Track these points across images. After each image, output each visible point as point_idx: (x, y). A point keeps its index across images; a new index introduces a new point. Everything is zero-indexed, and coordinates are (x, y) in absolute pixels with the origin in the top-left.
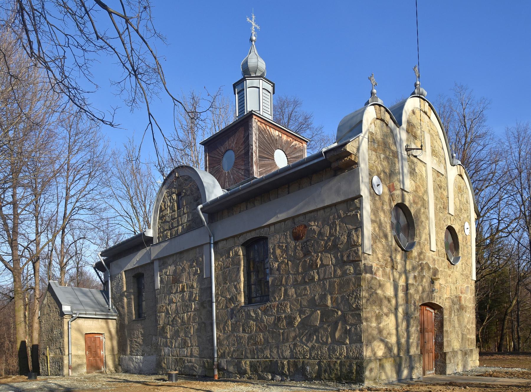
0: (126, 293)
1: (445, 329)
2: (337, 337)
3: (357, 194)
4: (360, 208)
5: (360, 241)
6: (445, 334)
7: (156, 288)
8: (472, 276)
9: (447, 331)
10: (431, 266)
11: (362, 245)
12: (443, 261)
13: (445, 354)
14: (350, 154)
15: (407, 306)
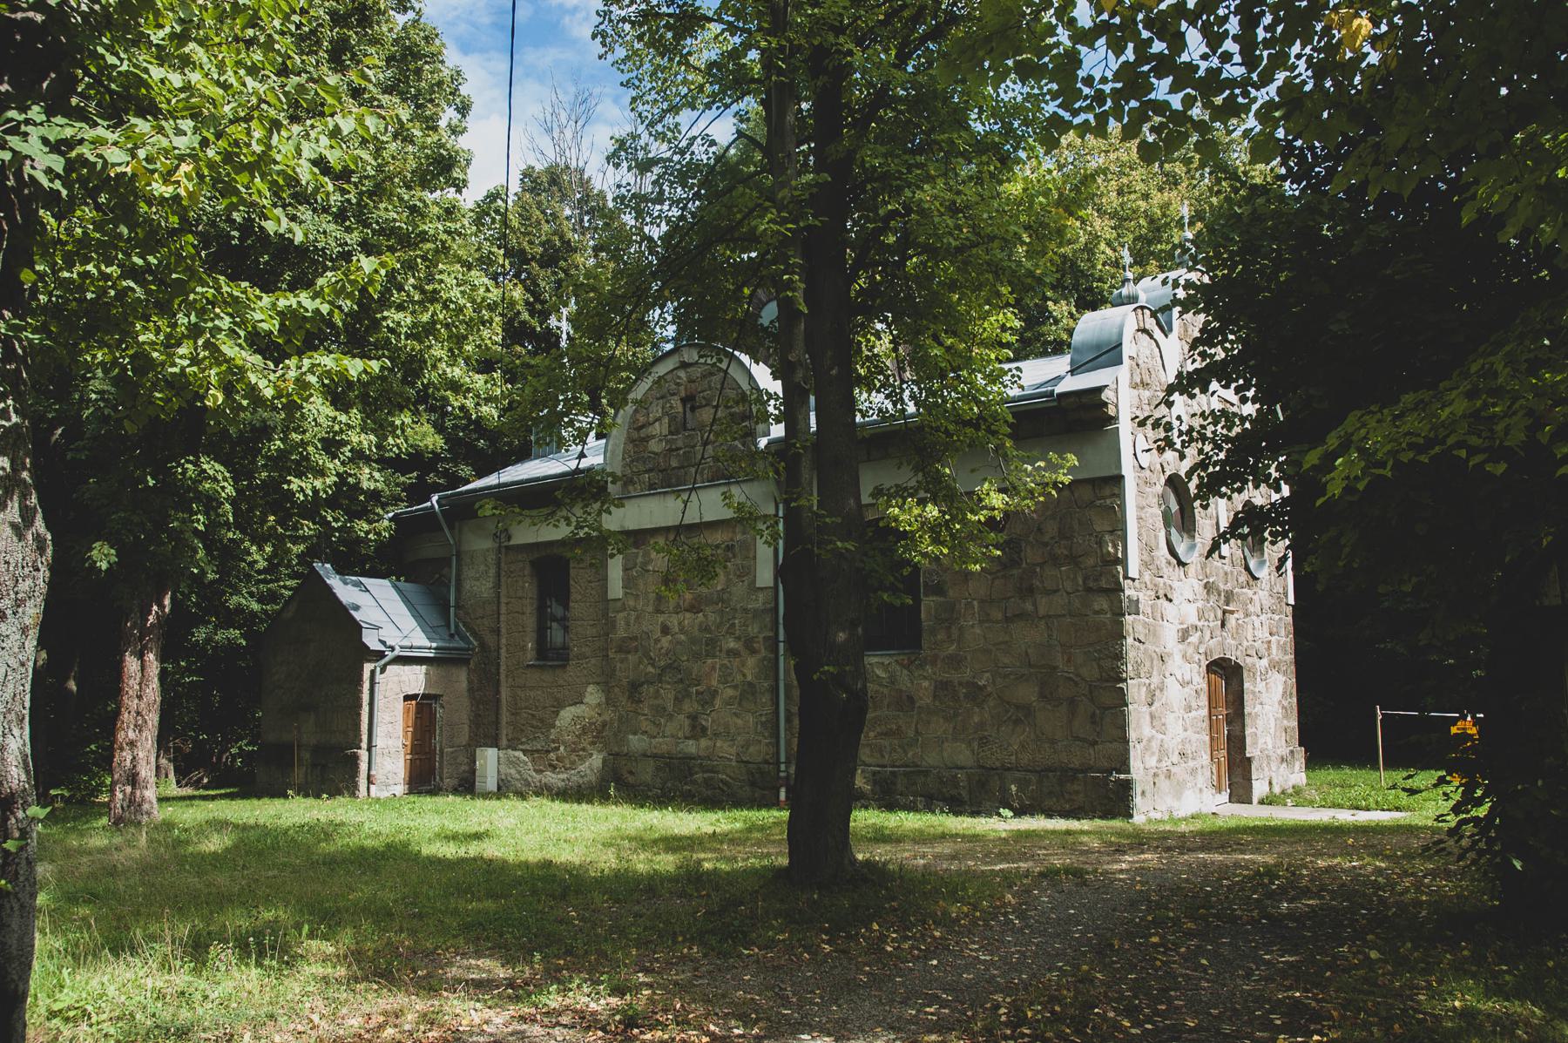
0: (103, 556)
1: (1247, 710)
2: (1505, 466)
3: (1116, 472)
4: (1121, 495)
5: (1120, 555)
6: (1248, 721)
7: (611, 595)
8: (1286, 597)
9: (1250, 714)
10: (1222, 587)
11: (1124, 562)
12: (1239, 573)
13: (1249, 760)
14: (1105, 404)
15: (870, 840)
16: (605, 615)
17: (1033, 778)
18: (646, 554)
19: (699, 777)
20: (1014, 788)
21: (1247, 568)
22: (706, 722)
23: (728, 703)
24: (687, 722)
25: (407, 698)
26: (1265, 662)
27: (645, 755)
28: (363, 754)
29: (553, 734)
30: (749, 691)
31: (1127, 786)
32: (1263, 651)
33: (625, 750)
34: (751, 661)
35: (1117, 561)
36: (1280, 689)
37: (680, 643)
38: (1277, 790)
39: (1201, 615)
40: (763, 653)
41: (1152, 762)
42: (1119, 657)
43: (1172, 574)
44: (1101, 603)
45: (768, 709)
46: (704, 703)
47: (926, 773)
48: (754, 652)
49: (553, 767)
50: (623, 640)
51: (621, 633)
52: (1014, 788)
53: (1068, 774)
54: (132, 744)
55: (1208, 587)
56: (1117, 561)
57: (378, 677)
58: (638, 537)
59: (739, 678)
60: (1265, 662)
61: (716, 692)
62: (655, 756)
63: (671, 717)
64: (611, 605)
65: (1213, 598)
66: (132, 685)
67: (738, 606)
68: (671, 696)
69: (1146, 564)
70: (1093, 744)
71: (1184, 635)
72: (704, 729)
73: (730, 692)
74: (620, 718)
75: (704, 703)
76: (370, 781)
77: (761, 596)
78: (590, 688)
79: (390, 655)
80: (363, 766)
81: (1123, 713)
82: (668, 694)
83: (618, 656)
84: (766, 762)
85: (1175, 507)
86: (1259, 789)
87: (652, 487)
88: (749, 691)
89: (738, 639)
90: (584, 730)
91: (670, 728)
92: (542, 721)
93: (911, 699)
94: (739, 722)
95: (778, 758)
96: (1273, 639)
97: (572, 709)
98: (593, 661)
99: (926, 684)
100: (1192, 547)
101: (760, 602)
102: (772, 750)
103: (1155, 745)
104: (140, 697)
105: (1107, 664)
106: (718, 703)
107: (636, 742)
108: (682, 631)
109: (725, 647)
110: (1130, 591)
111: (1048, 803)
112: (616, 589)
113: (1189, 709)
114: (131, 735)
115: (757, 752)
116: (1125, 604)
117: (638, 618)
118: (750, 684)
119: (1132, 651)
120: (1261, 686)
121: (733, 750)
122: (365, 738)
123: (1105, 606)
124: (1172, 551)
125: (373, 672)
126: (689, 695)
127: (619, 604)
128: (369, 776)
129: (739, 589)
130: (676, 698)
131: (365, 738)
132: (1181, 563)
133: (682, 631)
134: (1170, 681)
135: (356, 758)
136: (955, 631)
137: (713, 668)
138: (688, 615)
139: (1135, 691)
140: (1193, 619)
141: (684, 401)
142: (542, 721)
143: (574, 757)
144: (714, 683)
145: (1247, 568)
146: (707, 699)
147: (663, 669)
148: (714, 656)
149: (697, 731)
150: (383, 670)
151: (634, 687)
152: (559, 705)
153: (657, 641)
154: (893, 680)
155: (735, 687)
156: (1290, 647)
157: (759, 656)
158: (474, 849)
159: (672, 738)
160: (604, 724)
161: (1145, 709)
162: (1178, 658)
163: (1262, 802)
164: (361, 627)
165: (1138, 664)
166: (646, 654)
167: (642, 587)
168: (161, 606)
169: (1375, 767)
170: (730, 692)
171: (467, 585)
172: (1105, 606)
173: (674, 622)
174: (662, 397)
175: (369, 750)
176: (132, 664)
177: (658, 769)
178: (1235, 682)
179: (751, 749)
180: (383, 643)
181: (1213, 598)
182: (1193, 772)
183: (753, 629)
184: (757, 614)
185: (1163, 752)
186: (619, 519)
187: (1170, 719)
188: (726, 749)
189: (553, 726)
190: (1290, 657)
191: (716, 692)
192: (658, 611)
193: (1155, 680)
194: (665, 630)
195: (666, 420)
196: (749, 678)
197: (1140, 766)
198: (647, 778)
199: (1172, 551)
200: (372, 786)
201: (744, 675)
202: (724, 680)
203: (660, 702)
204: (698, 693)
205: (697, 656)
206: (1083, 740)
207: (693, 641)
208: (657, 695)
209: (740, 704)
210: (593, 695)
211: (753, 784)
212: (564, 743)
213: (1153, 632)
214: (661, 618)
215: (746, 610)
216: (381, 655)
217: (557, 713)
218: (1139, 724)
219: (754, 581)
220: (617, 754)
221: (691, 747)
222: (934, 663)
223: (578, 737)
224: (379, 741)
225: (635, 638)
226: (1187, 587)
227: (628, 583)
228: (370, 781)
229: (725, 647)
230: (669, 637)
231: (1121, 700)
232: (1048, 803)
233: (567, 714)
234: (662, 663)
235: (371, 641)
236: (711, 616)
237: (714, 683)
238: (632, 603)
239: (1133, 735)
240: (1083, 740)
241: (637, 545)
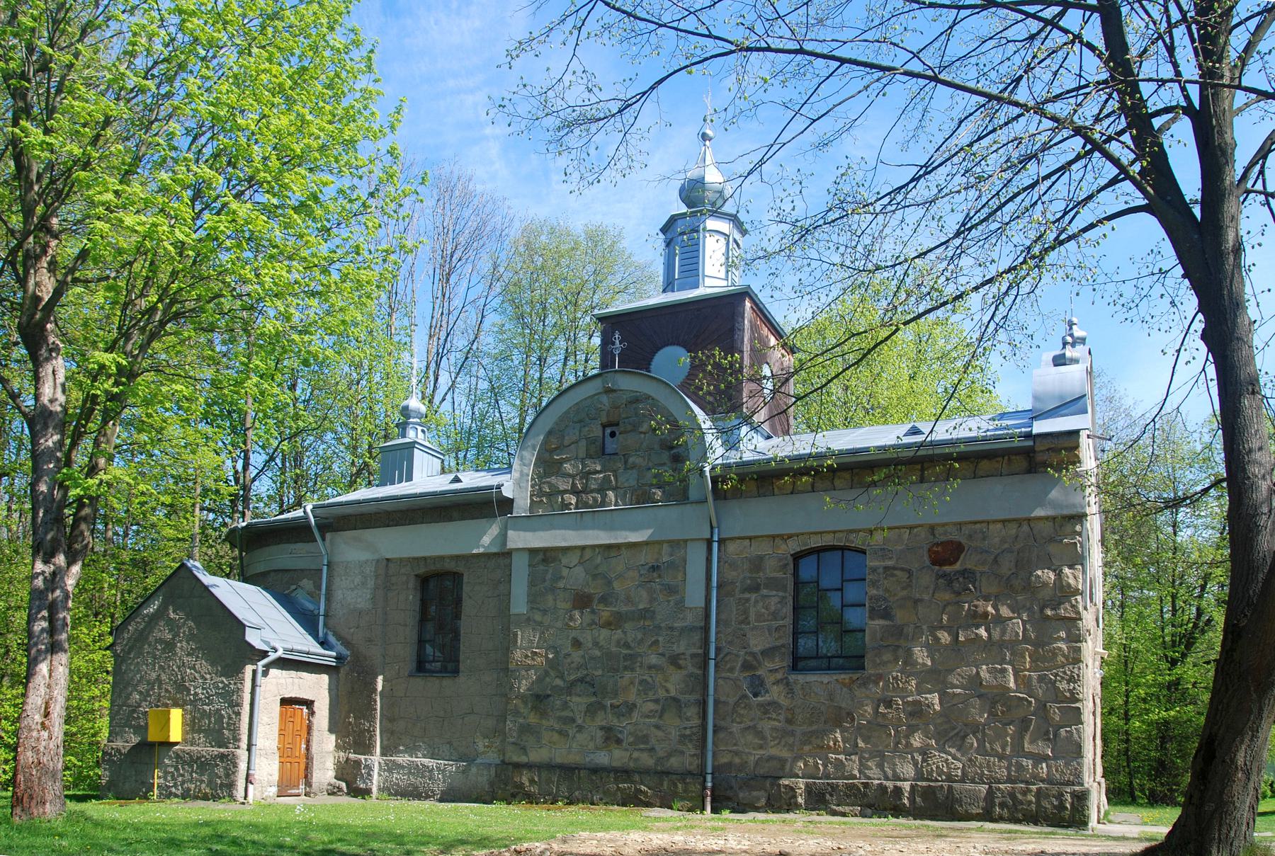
7: (514, 610)
24: (600, 734)
28: (242, 754)
40: (691, 669)
61: (634, 705)
67: (662, 625)
73: (651, 706)
79: (273, 656)
80: (243, 766)
102: (696, 762)
118: (675, 699)
122: (244, 738)
128: (248, 775)
131: (244, 738)
148: (633, 670)
150: (265, 674)
157: (684, 672)
158: (1098, 701)
164: (244, 626)
170: (651, 706)
171: (338, 595)
173: (587, 638)
174: (580, 421)
175: (249, 750)
183: (681, 647)
194: (577, 644)
195: (583, 443)
196: (673, 694)
201: (667, 691)
209: (660, 717)
216: (264, 654)
219: (682, 601)
227: (533, 599)
228: (248, 780)
230: (581, 652)
234: (572, 677)
235: (253, 638)
236: (631, 632)
241: (545, 561)
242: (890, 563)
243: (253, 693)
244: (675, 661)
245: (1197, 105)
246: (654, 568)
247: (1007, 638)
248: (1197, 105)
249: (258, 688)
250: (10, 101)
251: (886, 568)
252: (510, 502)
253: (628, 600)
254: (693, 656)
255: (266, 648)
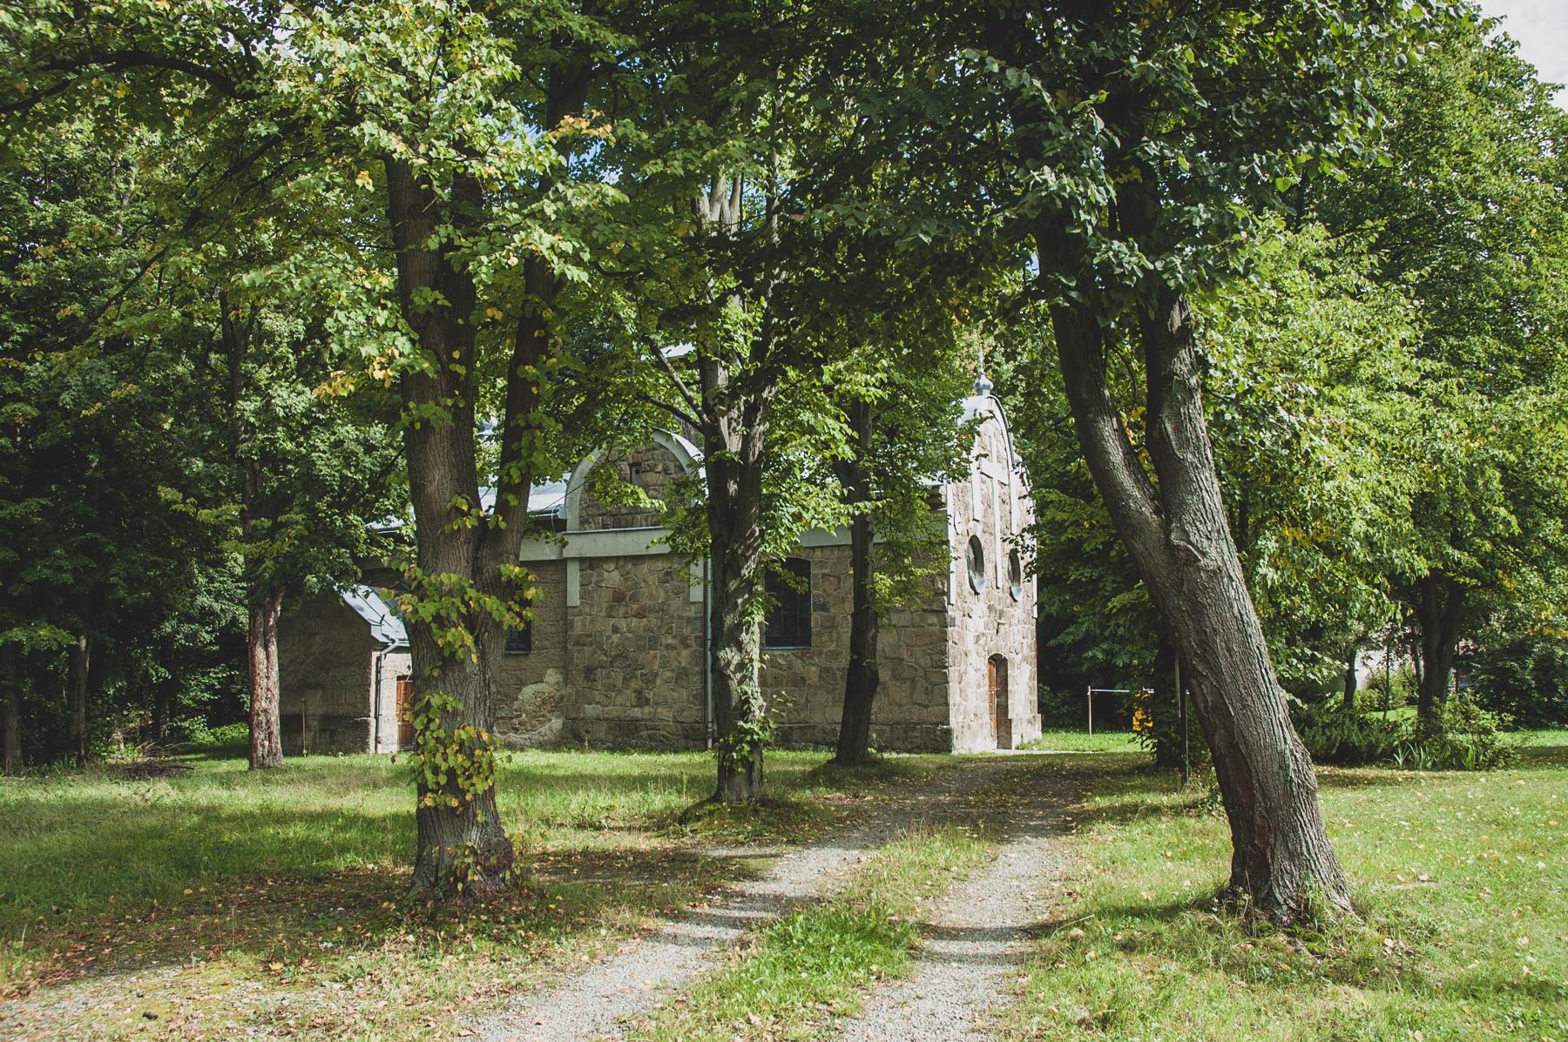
6: (1010, 695)
7: (569, 604)
11: (948, 594)
16: (565, 618)
17: (887, 728)
18: (601, 575)
19: (644, 733)
20: (874, 735)
21: (1011, 595)
22: (649, 695)
23: (666, 682)
24: (633, 695)
25: (399, 678)
26: (1020, 656)
27: (598, 719)
28: (372, 721)
29: (516, 705)
30: (682, 674)
31: (949, 732)
32: (1019, 650)
33: (582, 715)
34: (685, 653)
35: (944, 593)
36: (1028, 674)
37: (627, 639)
38: (1026, 741)
39: (986, 626)
40: (694, 647)
41: (960, 718)
42: (944, 653)
43: (971, 599)
44: (933, 619)
45: (699, 686)
46: (647, 682)
47: (814, 727)
48: (687, 646)
49: (516, 730)
50: (580, 636)
51: (578, 630)
52: (874, 735)
53: (910, 727)
54: (265, 711)
55: (990, 608)
56: (944, 593)
57: (384, 663)
58: (590, 563)
59: (675, 664)
60: (1020, 656)
61: (657, 674)
62: (607, 719)
63: (620, 692)
64: (569, 611)
65: (993, 615)
66: (262, 668)
68: (620, 677)
69: (959, 595)
70: (927, 707)
71: (978, 639)
72: (647, 701)
73: (668, 674)
74: (578, 692)
75: (647, 682)
76: (377, 741)
77: (693, 608)
78: (550, 671)
79: (392, 646)
80: (373, 730)
81: (946, 688)
82: (618, 676)
83: (576, 648)
84: (697, 722)
85: (972, 557)
86: (1016, 740)
87: (604, 526)
88: (682, 674)
89: (675, 637)
90: (544, 702)
91: (620, 699)
92: (506, 696)
93: (803, 679)
94: (676, 695)
95: (705, 716)
96: (1025, 641)
97: (534, 686)
98: (552, 651)
99: (814, 669)
100: (982, 582)
101: (692, 612)
103: (962, 708)
104: (268, 678)
105: (936, 657)
106: (658, 681)
107: (590, 710)
108: (629, 631)
109: (664, 642)
110: (951, 612)
111: (898, 744)
112: (574, 598)
113: (979, 686)
114: (264, 705)
115: (692, 714)
116: (949, 620)
117: (592, 621)
118: (684, 668)
119: (952, 649)
120: (1017, 671)
121: (671, 715)
123: (936, 621)
124: (972, 587)
125: (379, 659)
126: (635, 676)
127: (576, 610)
128: (377, 737)
129: (676, 603)
130: (624, 678)
132: (977, 593)
133: (629, 631)
134: (970, 668)
135: (367, 724)
136: (835, 635)
137: (655, 657)
138: (634, 619)
139: (953, 674)
140: (982, 629)
141: (631, 466)
142: (506, 696)
143: (534, 722)
144: (656, 667)
145: (1011, 595)
146: (650, 679)
147: (614, 658)
148: (655, 649)
149: (642, 701)
151: (589, 672)
152: (522, 684)
153: (609, 637)
154: (790, 666)
155: (673, 671)
156: (1034, 647)
159: (622, 705)
160: (562, 697)
161: (957, 685)
162: (974, 654)
163: (1017, 748)
165: (955, 658)
166: (600, 647)
167: (596, 598)
168: (276, 613)
169: (1086, 730)
170: (668, 674)
172: (936, 621)
173: (623, 624)
175: (376, 718)
176: (260, 653)
177: (611, 729)
178: (1002, 669)
179: (685, 713)
180: (387, 637)
181: (993, 615)
182: (982, 725)
183: (687, 631)
184: (689, 620)
185: (966, 714)
186: (579, 546)
187: (969, 692)
188: (663, 712)
189: (517, 699)
190: (1034, 653)
191: (657, 674)
192: (610, 616)
193: (962, 668)
194: (616, 630)
197: (955, 721)
198: (602, 735)
199: (972, 587)
200: (379, 746)
202: (664, 666)
203: (610, 681)
204: (642, 675)
205: (641, 649)
206: (920, 705)
207: (639, 638)
208: (608, 676)
210: (552, 676)
211: (687, 737)
212: (525, 711)
213: (961, 637)
214: (612, 621)
215: (680, 618)
216: (385, 646)
217: (520, 690)
218: (954, 698)
220: (575, 719)
221: (637, 713)
222: (820, 654)
223: (539, 707)
224: (383, 711)
225: (591, 635)
226: (979, 607)
227: (585, 595)
228: (377, 741)
229: (664, 642)
231: (945, 680)
232: (898, 744)
233: (528, 691)
236: (653, 621)
237: (656, 667)
238: (587, 610)
239: (951, 701)
240: (920, 705)
241: (591, 567)
242: (826, 571)
243: (378, 672)
244: (684, 642)
245: (824, 756)
246: (668, 573)
247: (992, 386)
248: (824, 756)
249: (383, 671)
250: (1541, 79)
251: (824, 575)
252: (565, 521)
253: (651, 596)
254: (696, 637)
255: (386, 640)
